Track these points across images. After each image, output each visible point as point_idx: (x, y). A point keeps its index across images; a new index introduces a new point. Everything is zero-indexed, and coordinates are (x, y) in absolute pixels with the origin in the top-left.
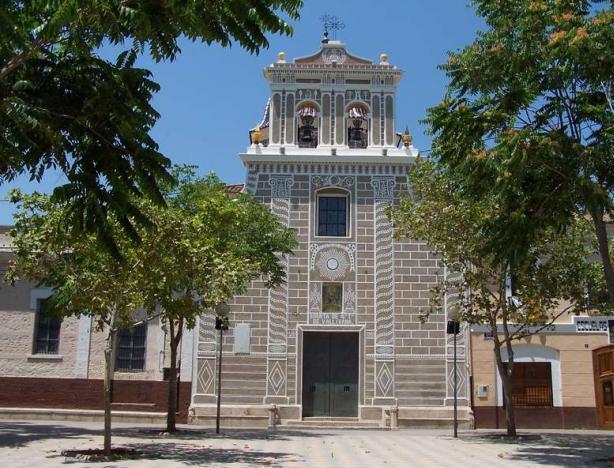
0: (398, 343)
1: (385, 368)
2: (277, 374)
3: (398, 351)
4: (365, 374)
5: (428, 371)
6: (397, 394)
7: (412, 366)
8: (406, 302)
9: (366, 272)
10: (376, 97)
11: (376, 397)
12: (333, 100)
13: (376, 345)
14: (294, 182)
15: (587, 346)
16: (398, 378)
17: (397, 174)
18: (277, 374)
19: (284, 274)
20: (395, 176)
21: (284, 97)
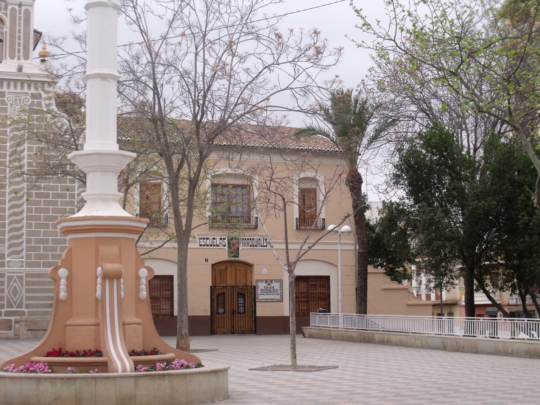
0: (28, 257)
1: (15, 281)
2: (15, 296)
3: (28, 265)
4: (329, 326)
5: (492, 329)
6: (27, 306)
7: (42, 280)
8: (38, 218)
9: (68, 190)
10: (13, 10)
11: (6, 309)
12: (20, 13)
13: (7, 259)
14: (30, 100)
15: (207, 260)
16: (28, 291)
17: (33, 91)
18: (15, 296)
19: (432, 219)
20: (30, 92)
21: (20, 11)
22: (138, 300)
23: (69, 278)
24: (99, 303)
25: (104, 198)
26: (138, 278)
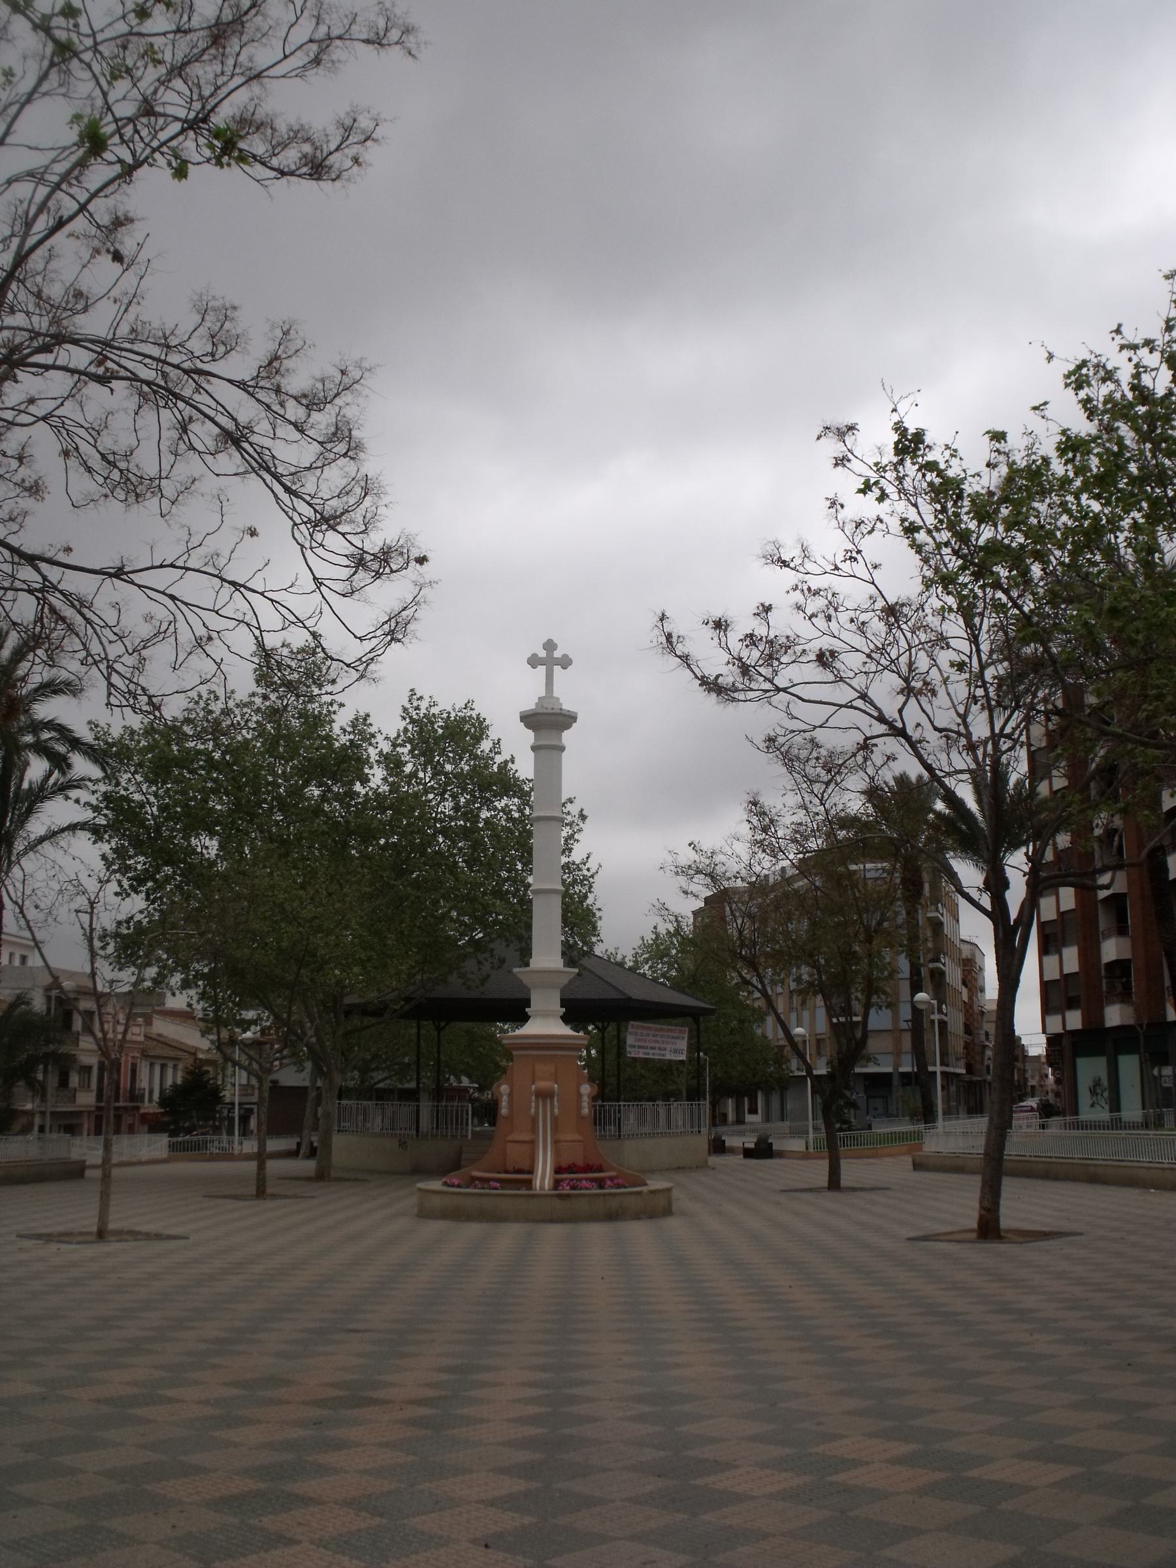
22: (581, 1118)
23: (510, 1095)
24: (534, 1121)
25: (546, 1015)
26: (580, 1096)
